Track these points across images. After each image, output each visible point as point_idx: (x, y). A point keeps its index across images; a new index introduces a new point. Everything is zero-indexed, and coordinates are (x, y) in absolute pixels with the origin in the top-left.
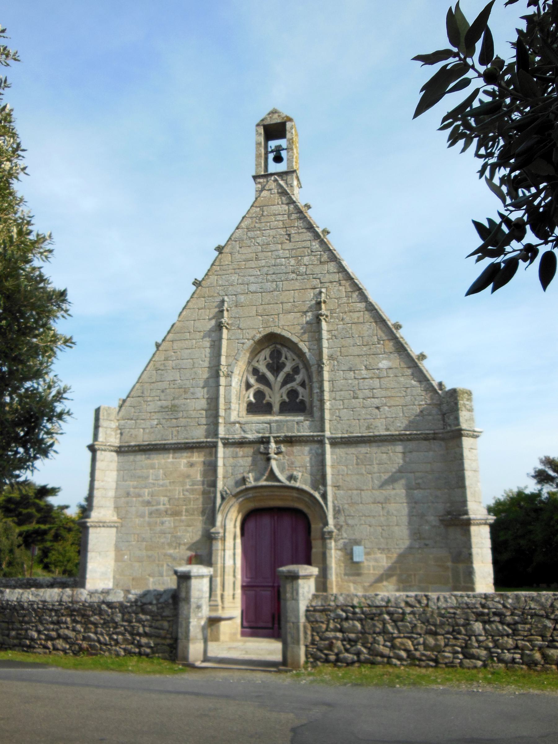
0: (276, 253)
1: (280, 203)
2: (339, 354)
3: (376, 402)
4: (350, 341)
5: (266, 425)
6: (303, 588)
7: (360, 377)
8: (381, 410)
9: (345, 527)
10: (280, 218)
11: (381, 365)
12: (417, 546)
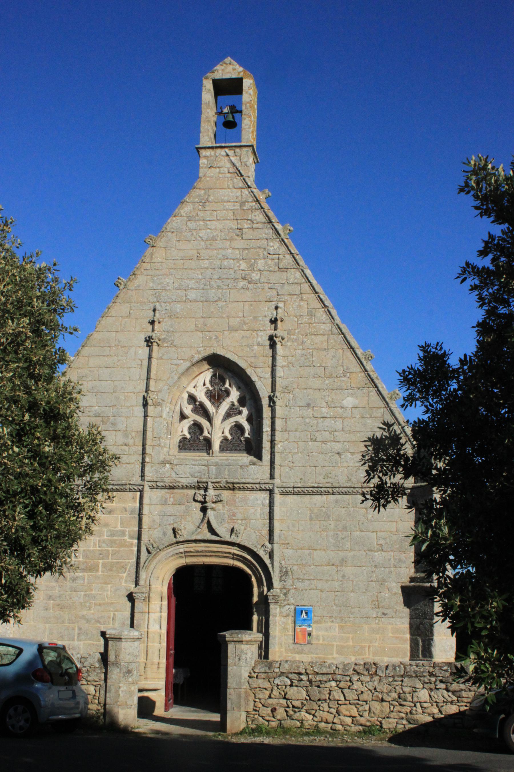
0: (223, 252)
1: (231, 186)
2: (295, 386)
3: (338, 447)
4: (311, 370)
5: (203, 467)
6: (246, 654)
7: (319, 416)
8: (343, 457)
9: (292, 591)
10: (229, 206)
11: (345, 403)
12: (374, 616)
